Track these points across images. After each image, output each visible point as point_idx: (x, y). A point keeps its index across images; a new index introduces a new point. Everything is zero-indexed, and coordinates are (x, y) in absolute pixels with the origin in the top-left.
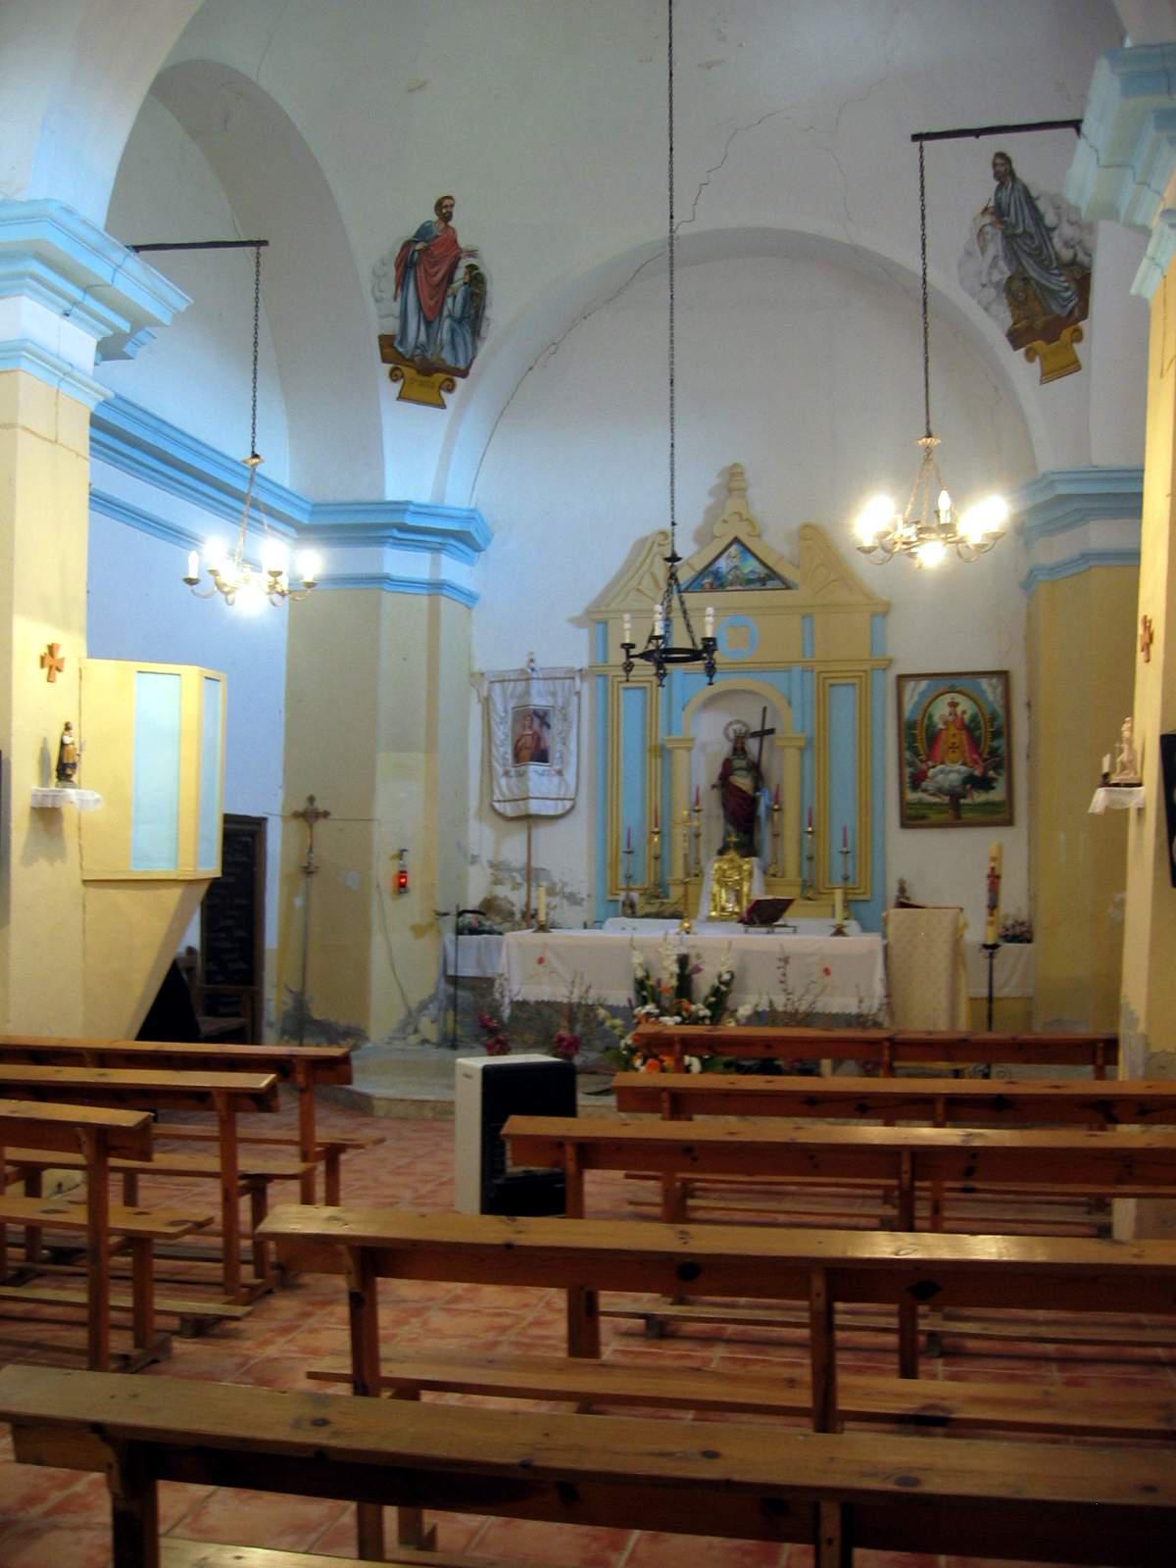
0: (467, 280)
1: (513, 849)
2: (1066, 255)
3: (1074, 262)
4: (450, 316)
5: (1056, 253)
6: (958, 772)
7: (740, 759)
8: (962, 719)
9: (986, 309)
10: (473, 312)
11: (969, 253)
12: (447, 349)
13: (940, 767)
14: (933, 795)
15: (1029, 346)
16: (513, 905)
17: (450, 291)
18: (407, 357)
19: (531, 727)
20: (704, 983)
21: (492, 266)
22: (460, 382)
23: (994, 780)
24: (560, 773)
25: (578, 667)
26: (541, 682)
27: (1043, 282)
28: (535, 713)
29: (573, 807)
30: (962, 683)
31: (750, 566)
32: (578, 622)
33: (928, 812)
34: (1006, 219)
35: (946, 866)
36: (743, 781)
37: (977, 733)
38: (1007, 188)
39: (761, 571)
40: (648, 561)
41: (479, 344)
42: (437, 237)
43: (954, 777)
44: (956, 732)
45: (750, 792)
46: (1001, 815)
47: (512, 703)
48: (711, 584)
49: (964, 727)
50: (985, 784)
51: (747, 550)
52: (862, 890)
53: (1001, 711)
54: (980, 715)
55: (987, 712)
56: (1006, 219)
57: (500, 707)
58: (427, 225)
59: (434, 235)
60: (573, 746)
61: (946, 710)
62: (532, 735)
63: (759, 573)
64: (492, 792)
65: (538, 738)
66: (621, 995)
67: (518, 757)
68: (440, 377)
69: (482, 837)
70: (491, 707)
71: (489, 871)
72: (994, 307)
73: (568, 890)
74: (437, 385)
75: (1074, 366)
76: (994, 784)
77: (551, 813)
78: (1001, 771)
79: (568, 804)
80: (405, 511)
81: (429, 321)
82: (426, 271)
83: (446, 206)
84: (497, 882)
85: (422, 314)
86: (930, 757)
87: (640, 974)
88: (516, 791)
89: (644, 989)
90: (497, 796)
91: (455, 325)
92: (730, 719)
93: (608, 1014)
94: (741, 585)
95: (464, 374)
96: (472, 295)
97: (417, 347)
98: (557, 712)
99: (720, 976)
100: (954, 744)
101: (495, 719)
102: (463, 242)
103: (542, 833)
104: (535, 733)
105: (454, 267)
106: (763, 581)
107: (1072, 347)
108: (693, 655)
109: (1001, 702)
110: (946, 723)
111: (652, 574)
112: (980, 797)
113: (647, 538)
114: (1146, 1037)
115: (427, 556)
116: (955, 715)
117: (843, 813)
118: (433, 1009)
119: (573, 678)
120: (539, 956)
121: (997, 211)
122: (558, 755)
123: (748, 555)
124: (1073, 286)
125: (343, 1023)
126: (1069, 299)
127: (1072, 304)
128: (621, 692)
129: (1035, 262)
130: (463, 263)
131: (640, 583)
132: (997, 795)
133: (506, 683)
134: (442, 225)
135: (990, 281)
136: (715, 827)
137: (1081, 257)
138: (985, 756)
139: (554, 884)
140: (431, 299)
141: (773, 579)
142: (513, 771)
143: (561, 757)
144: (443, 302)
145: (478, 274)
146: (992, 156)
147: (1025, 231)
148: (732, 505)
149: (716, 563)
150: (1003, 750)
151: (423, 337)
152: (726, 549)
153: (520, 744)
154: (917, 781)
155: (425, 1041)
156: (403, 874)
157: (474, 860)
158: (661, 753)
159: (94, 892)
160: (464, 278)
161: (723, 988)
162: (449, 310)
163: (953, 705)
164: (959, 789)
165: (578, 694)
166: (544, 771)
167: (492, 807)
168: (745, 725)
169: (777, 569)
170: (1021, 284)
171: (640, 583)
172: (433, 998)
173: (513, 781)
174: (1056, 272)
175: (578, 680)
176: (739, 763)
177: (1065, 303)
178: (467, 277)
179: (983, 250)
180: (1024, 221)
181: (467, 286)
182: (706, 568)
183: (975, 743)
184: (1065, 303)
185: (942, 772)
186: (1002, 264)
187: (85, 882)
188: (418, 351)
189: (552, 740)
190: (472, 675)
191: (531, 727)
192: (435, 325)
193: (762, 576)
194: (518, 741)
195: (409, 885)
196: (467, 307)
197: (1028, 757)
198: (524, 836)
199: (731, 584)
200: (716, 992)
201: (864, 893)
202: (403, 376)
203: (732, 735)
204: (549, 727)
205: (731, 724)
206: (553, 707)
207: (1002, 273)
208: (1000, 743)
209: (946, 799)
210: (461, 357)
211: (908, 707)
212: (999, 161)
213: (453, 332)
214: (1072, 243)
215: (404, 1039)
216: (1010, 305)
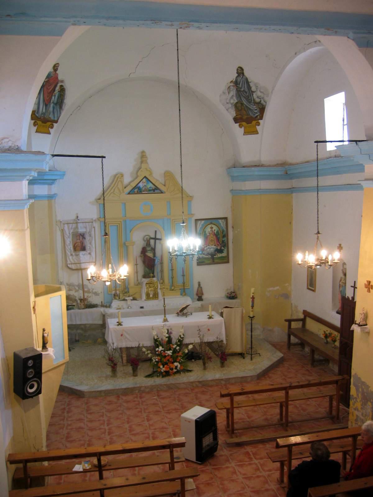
0: (59, 90)
2: (258, 100)
3: (260, 103)
4: (53, 102)
5: (254, 99)
6: (213, 248)
7: (149, 247)
8: (214, 232)
9: (227, 110)
10: (60, 101)
11: (224, 93)
12: (52, 113)
14: (206, 255)
15: (240, 123)
16: (76, 297)
17: (54, 95)
18: (39, 117)
19: (79, 239)
20: (174, 340)
21: (67, 86)
22: (55, 125)
23: (224, 250)
24: (90, 254)
26: (81, 224)
27: (247, 105)
28: (80, 234)
31: (150, 185)
34: (238, 85)
36: (150, 254)
37: (219, 236)
38: (240, 77)
39: (154, 187)
40: (116, 184)
41: (62, 111)
42: (52, 76)
43: (212, 249)
44: (213, 236)
45: (153, 258)
46: (226, 260)
47: (72, 231)
48: (137, 191)
50: (221, 251)
52: (187, 285)
53: (225, 229)
54: (219, 231)
56: (238, 85)
58: (50, 73)
59: (51, 76)
61: (210, 230)
62: (80, 242)
63: (153, 188)
65: (82, 243)
67: (75, 249)
68: (49, 123)
70: (64, 232)
71: (67, 287)
72: (230, 110)
73: (94, 291)
74: (48, 127)
75: (256, 132)
76: (224, 251)
78: (225, 247)
80: (44, 175)
81: (46, 105)
82: (47, 88)
83: (57, 67)
84: (70, 290)
85: (44, 102)
87: (156, 338)
91: (55, 106)
93: (146, 350)
94: (147, 191)
95: (56, 122)
96: (61, 95)
97: (42, 114)
98: (87, 234)
99: (180, 336)
100: (212, 240)
101: (66, 236)
102: (60, 78)
104: (81, 241)
105: (56, 86)
106: (154, 190)
107: (256, 127)
109: (225, 227)
110: (209, 233)
111: (118, 188)
112: (219, 255)
115: (46, 186)
116: (212, 231)
119: (93, 222)
120: (121, 333)
121: (236, 83)
122: (89, 248)
123: (149, 182)
124: (258, 109)
126: (256, 113)
127: (257, 114)
128: (110, 227)
129: (246, 100)
130: (59, 85)
132: (224, 254)
133: (69, 224)
134: (54, 73)
135: (230, 103)
137: (262, 102)
138: (221, 243)
140: (48, 97)
141: (157, 190)
142: (74, 254)
143: (90, 248)
144: (51, 98)
145: (63, 88)
146: (237, 67)
147: (244, 90)
149: (139, 184)
150: (226, 241)
151: (44, 111)
152: (142, 180)
153: (76, 245)
160: (59, 90)
162: (53, 101)
163: (212, 228)
165: (94, 227)
166: (85, 253)
167: (68, 266)
170: (240, 105)
173: (74, 257)
174: (253, 104)
175: (94, 222)
177: (255, 114)
178: (60, 89)
179: (229, 93)
180: (244, 87)
181: (59, 92)
182: (135, 186)
183: (218, 239)
184: (255, 114)
185: (208, 248)
186: (235, 98)
188: (43, 115)
191: (79, 239)
192: (48, 105)
193: (154, 188)
194: (75, 244)
196: (59, 100)
197: (233, 242)
199: (144, 191)
200: (179, 341)
201: (188, 286)
202: (37, 124)
205: (145, 236)
206: (86, 232)
207: (234, 100)
208: (225, 239)
209: (210, 256)
210: (56, 116)
212: (239, 69)
213: (54, 108)
214: (260, 97)
216: (235, 110)
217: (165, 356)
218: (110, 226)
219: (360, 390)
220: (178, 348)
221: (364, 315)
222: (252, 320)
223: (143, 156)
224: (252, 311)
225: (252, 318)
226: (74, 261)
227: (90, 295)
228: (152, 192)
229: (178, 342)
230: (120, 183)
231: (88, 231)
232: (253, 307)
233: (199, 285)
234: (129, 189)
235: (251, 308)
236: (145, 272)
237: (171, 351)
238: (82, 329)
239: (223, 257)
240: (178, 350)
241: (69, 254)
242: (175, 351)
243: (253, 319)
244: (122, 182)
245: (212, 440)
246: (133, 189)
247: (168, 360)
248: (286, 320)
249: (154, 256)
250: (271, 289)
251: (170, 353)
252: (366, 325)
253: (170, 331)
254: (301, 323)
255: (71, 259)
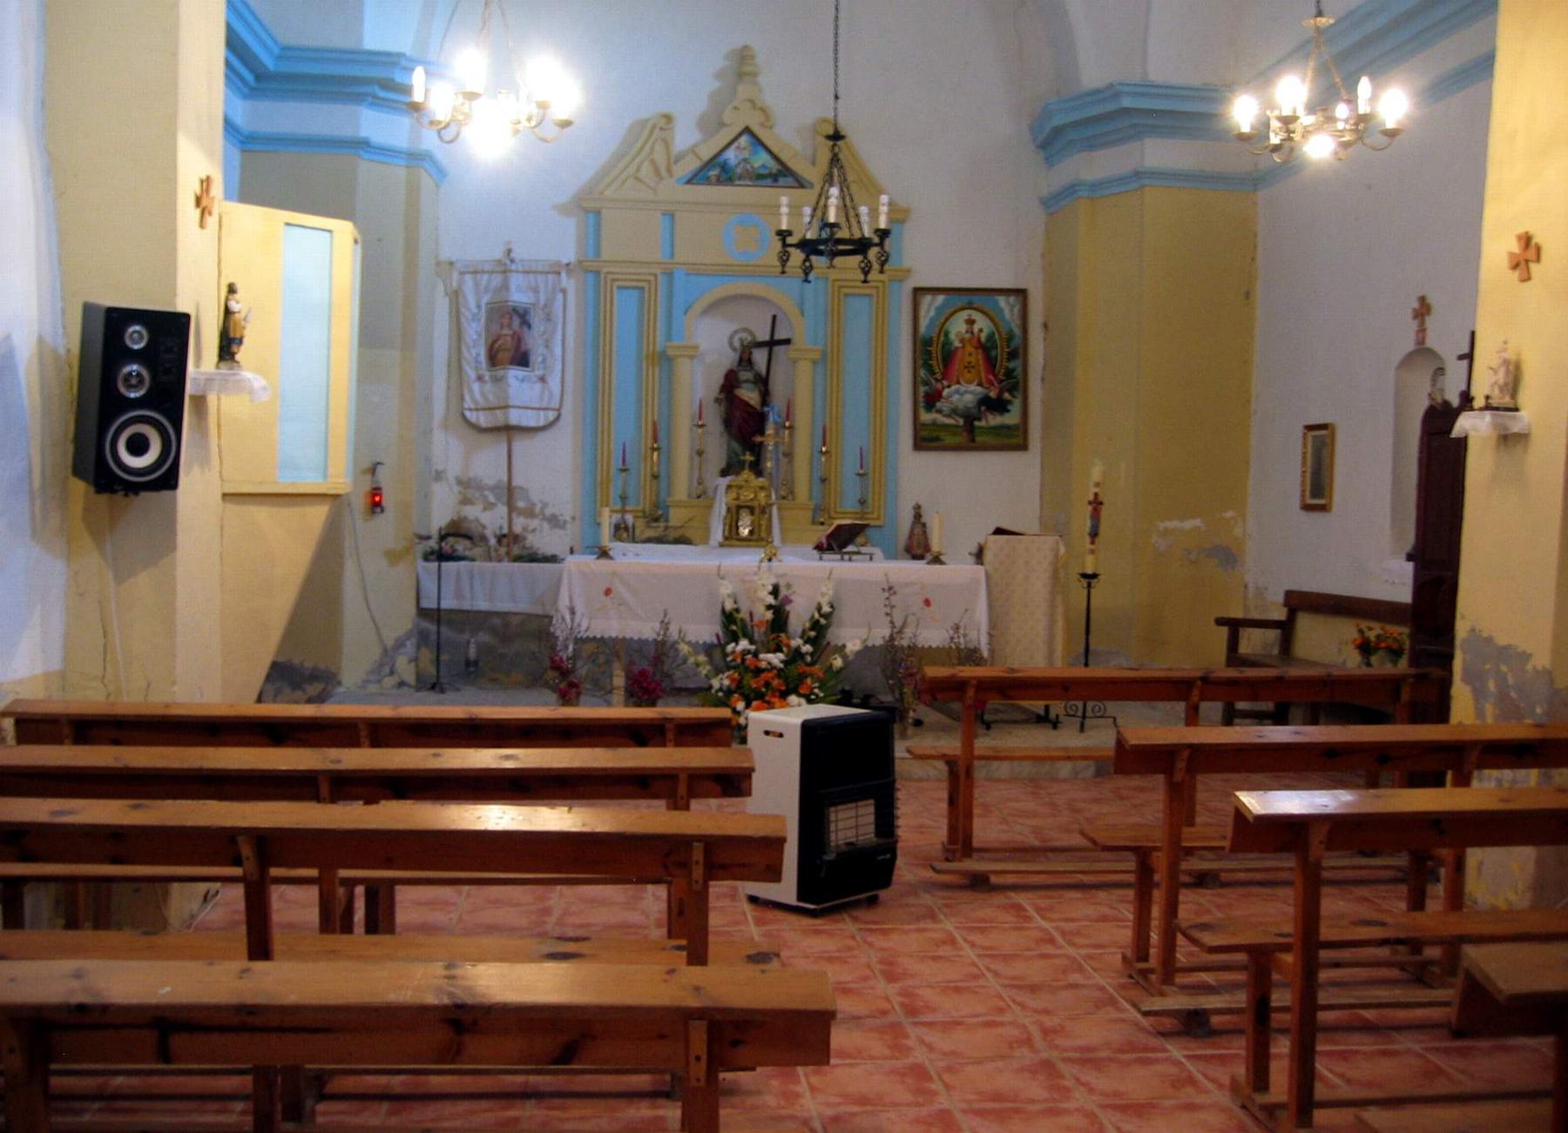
1: (488, 463)
13: (954, 387)
14: (948, 416)
16: (484, 527)
19: (510, 326)
20: (799, 617)
23: (1009, 402)
24: (542, 379)
25: (565, 261)
28: (515, 310)
29: (558, 418)
30: (977, 300)
31: (761, 160)
32: (564, 210)
33: (942, 435)
35: (964, 491)
36: (749, 395)
46: (1014, 440)
47: (486, 299)
49: (980, 345)
50: (999, 406)
51: (758, 142)
53: (1017, 331)
55: (1004, 331)
57: (472, 300)
60: (558, 351)
61: (963, 327)
64: (462, 398)
65: (518, 340)
66: (706, 630)
67: (493, 359)
69: (447, 450)
70: (461, 300)
71: (456, 489)
73: (548, 512)
77: (532, 424)
79: (551, 415)
84: (466, 501)
86: (945, 376)
87: (729, 606)
88: (491, 397)
89: (732, 623)
90: (468, 403)
92: (734, 328)
99: (819, 609)
103: (521, 445)
108: (861, 246)
110: (962, 341)
111: (653, 162)
112: (994, 420)
113: (647, 120)
114: (1550, 673)
117: (854, 437)
118: (410, 646)
125: (308, 665)
131: (638, 170)
132: (1012, 418)
136: (717, 447)
139: (534, 504)
143: (544, 361)
148: (744, 90)
150: (1019, 371)
154: (932, 400)
155: (402, 684)
156: (376, 491)
157: (439, 476)
158: (663, 361)
159: (234, 509)
161: (823, 621)
163: (971, 322)
164: (975, 411)
165: (564, 291)
167: (463, 415)
168: (750, 333)
169: (790, 164)
171: (638, 170)
172: (408, 636)
173: (488, 387)
175: (563, 274)
176: (745, 375)
183: (991, 363)
185: (957, 392)
187: (225, 495)
189: (534, 342)
190: (438, 264)
191: (510, 326)
194: (495, 342)
195: (384, 503)
197: (1043, 379)
198: (505, 446)
199: (740, 178)
200: (815, 625)
203: (737, 344)
204: (530, 327)
205: (736, 332)
209: (961, 422)
211: (924, 323)
215: (379, 681)
217: (758, 671)
218: (619, 288)
219: (1491, 685)
220: (807, 648)
221: (1508, 371)
222: (1089, 585)
223: (742, 66)
224: (1092, 552)
225: (1090, 577)
226: (486, 399)
227: (534, 523)
228: (769, 181)
229: (812, 628)
230: (659, 147)
231: (542, 301)
232: (1094, 534)
233: (918, 516)
234: (692, 165)
235: (1088, 539)
236: (729, 457)
237: (781, 656)
238: (493, 631)
239: (1008, 427)
240: (809, 659)
241: (471, 373)
242: (796, 655)
243: (1094, 582)
244: (667, 144)
245: (872, 828)
246: (701, 169)
247: (767, 684)
248: (1220, 622)
249: (765, 396)
250: (1171, 524)
251: (776, 659)
252: (1517, 410)
253: (783, 592)
254: (1273, 635)
255: (476, 392)
